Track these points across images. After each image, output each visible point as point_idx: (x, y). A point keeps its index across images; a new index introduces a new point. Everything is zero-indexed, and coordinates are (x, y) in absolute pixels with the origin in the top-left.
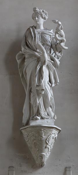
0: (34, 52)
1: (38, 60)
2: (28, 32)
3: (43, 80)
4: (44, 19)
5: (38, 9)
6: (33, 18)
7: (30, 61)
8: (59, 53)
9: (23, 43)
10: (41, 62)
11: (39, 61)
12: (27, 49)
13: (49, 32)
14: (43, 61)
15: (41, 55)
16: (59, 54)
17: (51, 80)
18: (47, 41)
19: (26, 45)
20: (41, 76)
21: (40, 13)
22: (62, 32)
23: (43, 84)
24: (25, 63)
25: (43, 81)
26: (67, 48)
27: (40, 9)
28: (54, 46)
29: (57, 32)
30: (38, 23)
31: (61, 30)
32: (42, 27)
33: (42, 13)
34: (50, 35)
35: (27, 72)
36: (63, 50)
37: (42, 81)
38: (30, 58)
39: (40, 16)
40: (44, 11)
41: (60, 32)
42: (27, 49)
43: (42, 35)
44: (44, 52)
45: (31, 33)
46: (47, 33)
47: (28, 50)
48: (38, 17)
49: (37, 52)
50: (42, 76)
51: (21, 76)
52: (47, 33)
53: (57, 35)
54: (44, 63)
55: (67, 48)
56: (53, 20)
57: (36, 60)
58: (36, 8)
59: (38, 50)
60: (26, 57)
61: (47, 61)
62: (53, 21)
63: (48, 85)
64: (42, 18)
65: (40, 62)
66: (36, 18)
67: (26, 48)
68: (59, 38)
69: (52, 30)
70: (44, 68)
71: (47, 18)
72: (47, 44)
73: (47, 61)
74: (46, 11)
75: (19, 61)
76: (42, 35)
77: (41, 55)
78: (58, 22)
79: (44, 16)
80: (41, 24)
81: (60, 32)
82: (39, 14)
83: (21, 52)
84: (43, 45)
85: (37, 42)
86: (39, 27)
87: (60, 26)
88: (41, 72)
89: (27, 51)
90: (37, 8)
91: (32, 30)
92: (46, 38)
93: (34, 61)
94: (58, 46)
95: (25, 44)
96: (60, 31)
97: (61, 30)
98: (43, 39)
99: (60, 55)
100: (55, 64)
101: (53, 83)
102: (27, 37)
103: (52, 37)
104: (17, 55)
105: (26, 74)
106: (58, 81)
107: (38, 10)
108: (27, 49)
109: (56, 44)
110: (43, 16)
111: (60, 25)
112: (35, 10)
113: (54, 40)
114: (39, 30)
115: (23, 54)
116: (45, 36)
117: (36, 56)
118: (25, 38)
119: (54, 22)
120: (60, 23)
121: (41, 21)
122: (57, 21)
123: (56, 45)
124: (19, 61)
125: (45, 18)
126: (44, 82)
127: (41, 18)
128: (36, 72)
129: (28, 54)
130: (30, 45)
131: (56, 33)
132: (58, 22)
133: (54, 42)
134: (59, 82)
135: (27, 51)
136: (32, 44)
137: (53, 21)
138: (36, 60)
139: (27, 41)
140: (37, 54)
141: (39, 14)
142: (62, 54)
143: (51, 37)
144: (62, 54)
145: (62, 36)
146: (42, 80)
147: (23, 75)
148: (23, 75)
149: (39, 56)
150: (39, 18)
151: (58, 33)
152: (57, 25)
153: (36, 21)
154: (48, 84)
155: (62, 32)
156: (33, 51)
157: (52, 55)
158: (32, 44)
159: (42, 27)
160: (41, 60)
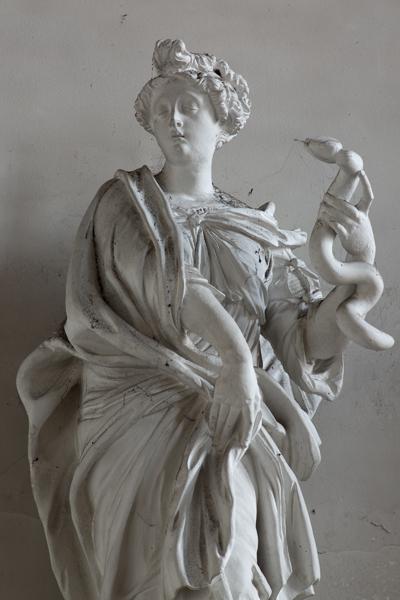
0: (168, 352)
1: (190, 410)
2: (109, 207)
3: (229, 554)
4: (223, 123)
5: (185, 57)
6: (144, 117)
7: (133, 416)
8: (317, 371)
9: (75, 282)
10: (214, 429)
11: (190, 414)
12: (108, 329)
13: (259, 222)
14: (230, 422)
15: (209, 379)
16: (320, 382)
17: (271, 552)
18: (246, 280)
19: (98, 300)
20: (208, 524)
21: (203, 82)
22: (365, 227)
23: (226, 584)
24: (85, 432)
25: (225, 561)
26: (386, 340)
27: (198, 57)
28: (288, 320)
29: (329, 222)
30: (186, 148)
31: (359, 214)
32: (206, 186)
33: (219, 85)
34: (264, 244)
35: (97, 488)
36: (351, 350)
37: (218, 564)
38: (133, 388)
39: (201, 99)
40: (228, 70)
41: (349, 228)
42: (115, 328)
43: (213, 236)
44: (238, 360)
45: (134, 214)
46: (245, 222)
47: (117, 337)
48: (184, 111)
49: (185, 354)
50: (215, 523)
51: (43, 513)
52: (245, 222)
53: (328, 246)
54: (238, 429)
55: (386, 340)
56: (312, 136)
57: (170, 407)
58: (176, 46)
59: (189, 342)
60: (93, 377)
61: (257, 422)
62: (307, 143)
63: (254, 592)
64: (217, 116)
65: (205, 428)
66: (178, 117)
67: (107, 316)
68: (345, 270)
69: (271, 209)
70: (234, 463)
71: (243, 119)
72: (245, 299)
73: (257, 422)
74: (231, 68)
75: (36, 412)
76: (215, 233)
77: (209, 379)
78: (344, 153)
79: (231, 105)
80: (202, 160)
81: (349, 228)
82: (196, 86)
83: (55, 344)
84: (226, 303)
85: (190, 282)
86: (190, 183)
87: (358, 180)
88: (208, 497)
89: (108, 338)
90: (183, 46)
91: (140, 197)
92: (241, 258)
93: (159, 416)
94: (318, 324)
95: (95, 293)
96: (350, 221)
97: (359, 214)
98: (215, 264)
99: (327, 389)
100: (292, 446)
101: (285, 582)
102: (103, 240)
103: (277, 258)
104: (25, 366)
105: (88, 511)
106: (313, 573)
107: (187, 59)
108: (108, 329)
109: (304, 306)
110: (224, 105)
111: (358, 174)
112: (164, 58)
113: (291, 278)
114: (186, 197)
115: (70, 361)
116: (231, 242)
117: (169, 380)
118: (86, 247)
119: (321, 151)
120: (357, 161)
121: (209, 137)
122: (339, 147)
123: (303, 315)
124: (36, 412)
125: (228, 123)
126: (235, 565)
127: (206, 118)
128: (168, 494)
129: (116, 359)
130: (134, 301)
131: (323, 228)
132: (344, 153)
133: (290, 295)
134: (318, 575)
135: (114, 340)
136: (151, 293)
137: (307, 143)
138: (174, 412)
139: (109, 275)
140: (181, 363)
141: (196, 86)
142: (340, 384)
143: (273, 253)
144: (340, 384)
145: (354, 254)
146: (223, 551)
147: (59, 508)
148: (59, 508)
149: (199, 379)
150: (195, 118)
151: (334, 233)
152: (332, 170)
153: (176, 136)
154: (255, 583)
155: (365, 227)
156: (153, 344)
157: (267, 370)
158: (153, 294)
159: (206, 186)
160: (213, 412)
